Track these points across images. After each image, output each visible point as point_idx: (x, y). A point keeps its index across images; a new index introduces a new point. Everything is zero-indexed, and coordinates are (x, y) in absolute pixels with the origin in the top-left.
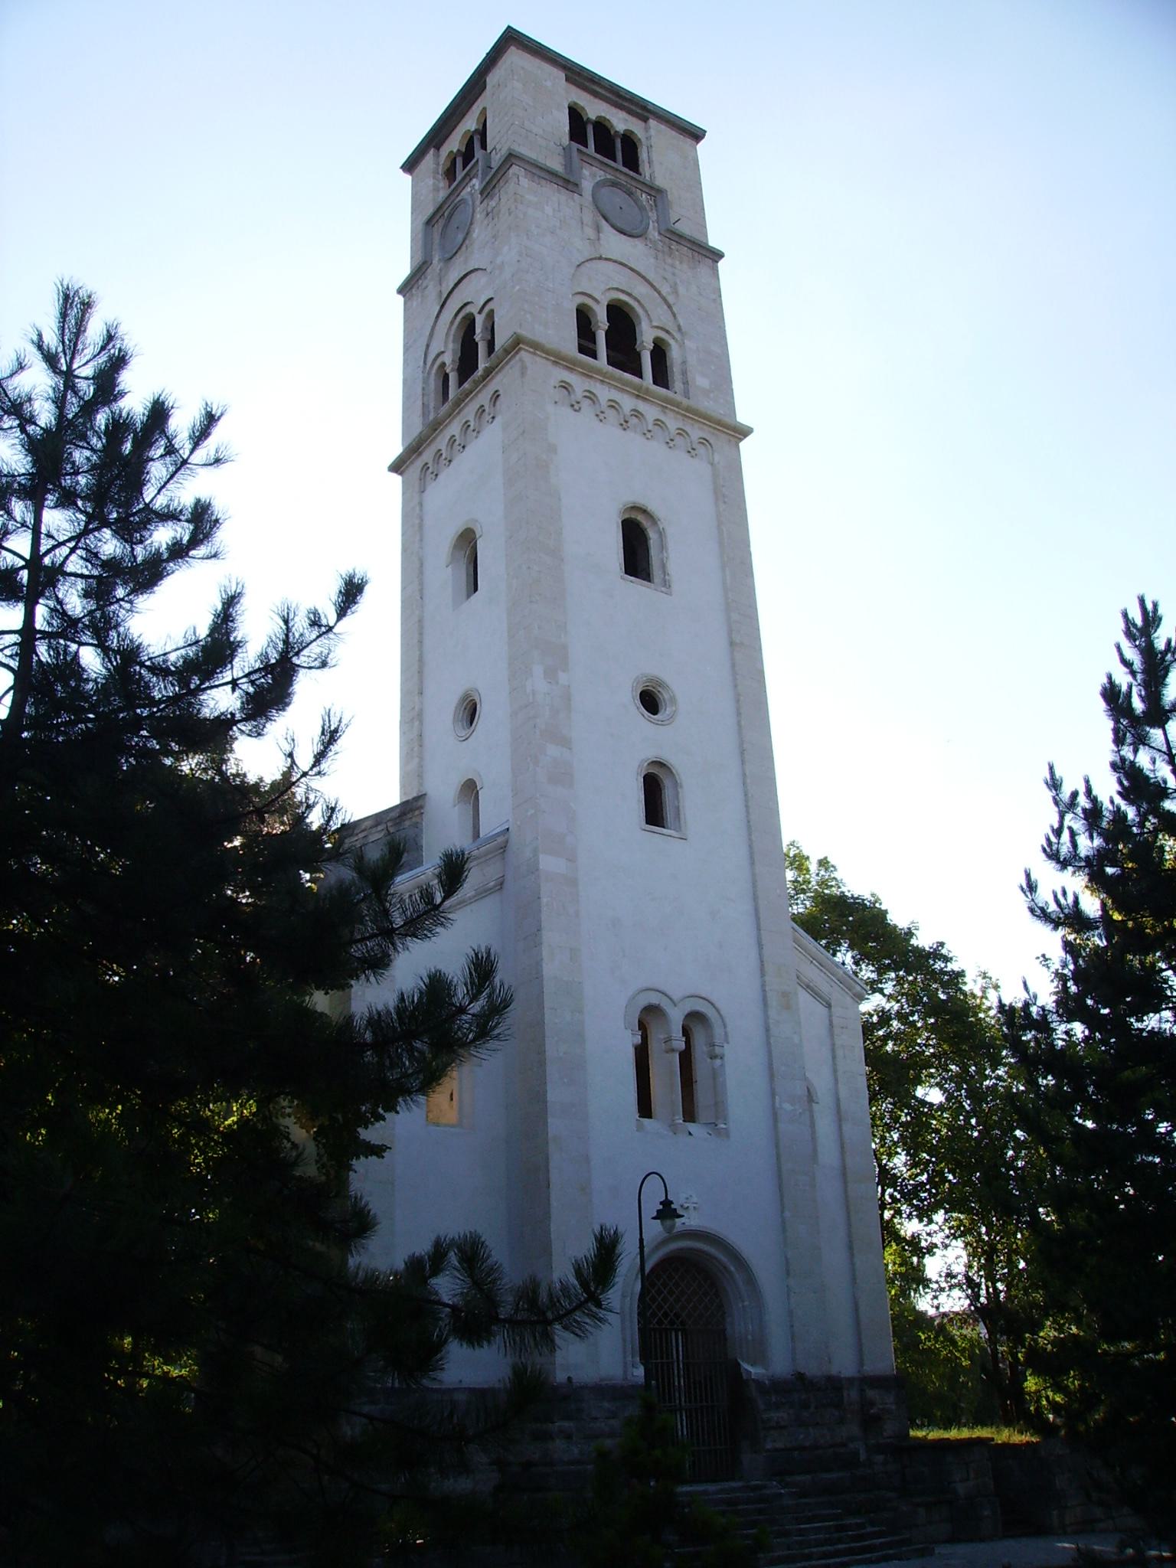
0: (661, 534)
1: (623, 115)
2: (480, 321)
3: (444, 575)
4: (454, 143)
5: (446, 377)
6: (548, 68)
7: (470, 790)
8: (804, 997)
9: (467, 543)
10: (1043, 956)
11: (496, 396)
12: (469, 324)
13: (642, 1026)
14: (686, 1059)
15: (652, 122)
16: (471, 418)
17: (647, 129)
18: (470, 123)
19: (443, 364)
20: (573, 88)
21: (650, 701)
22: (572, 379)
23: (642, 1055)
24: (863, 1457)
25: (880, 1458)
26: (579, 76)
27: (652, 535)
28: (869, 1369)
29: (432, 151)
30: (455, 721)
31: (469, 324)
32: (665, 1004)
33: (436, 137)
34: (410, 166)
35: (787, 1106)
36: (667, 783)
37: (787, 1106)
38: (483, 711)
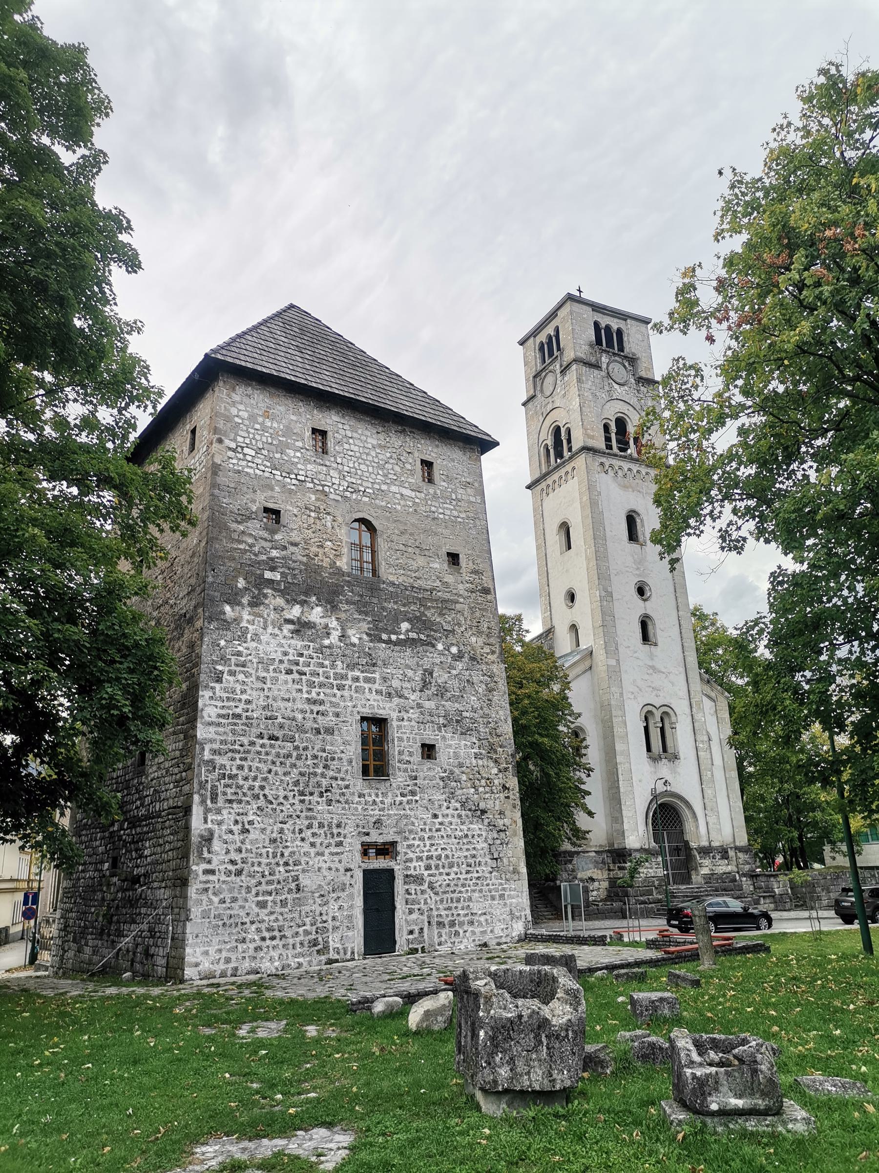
0: (642, 521)
1: (616, 320)
2: (563, 430)
3: (555, 539)
4: (542, 337)
5: (548, 451)
6: (584, 307)
7: (574, 628)
8: (705, 699)
9: (565, 528)
10: (674, 359)
11: (574, 468)
12: (557, 430)
13: (646, 719)
14: (662, 730)
15: (629, 321)
16: (563, 475)
17: (627, 325)
18: (550, 330)
19: (547, 445)
20: (595, 313)
21: (641, 591)
22: (604, 460)
23: (646, 729)
24: (738, 878)
25: (744, 879)
26: (597, 308)
27: (638, 520)
28: (738, 844)
29: (532, 338)
30: (565, 600)
31: (557, 430)
32: (654, 710)
33: (534, 333)
34: (522, 343)
35: (701, 745)
36: (649, 623)
37: (701, 745)
38: (577, 598)
